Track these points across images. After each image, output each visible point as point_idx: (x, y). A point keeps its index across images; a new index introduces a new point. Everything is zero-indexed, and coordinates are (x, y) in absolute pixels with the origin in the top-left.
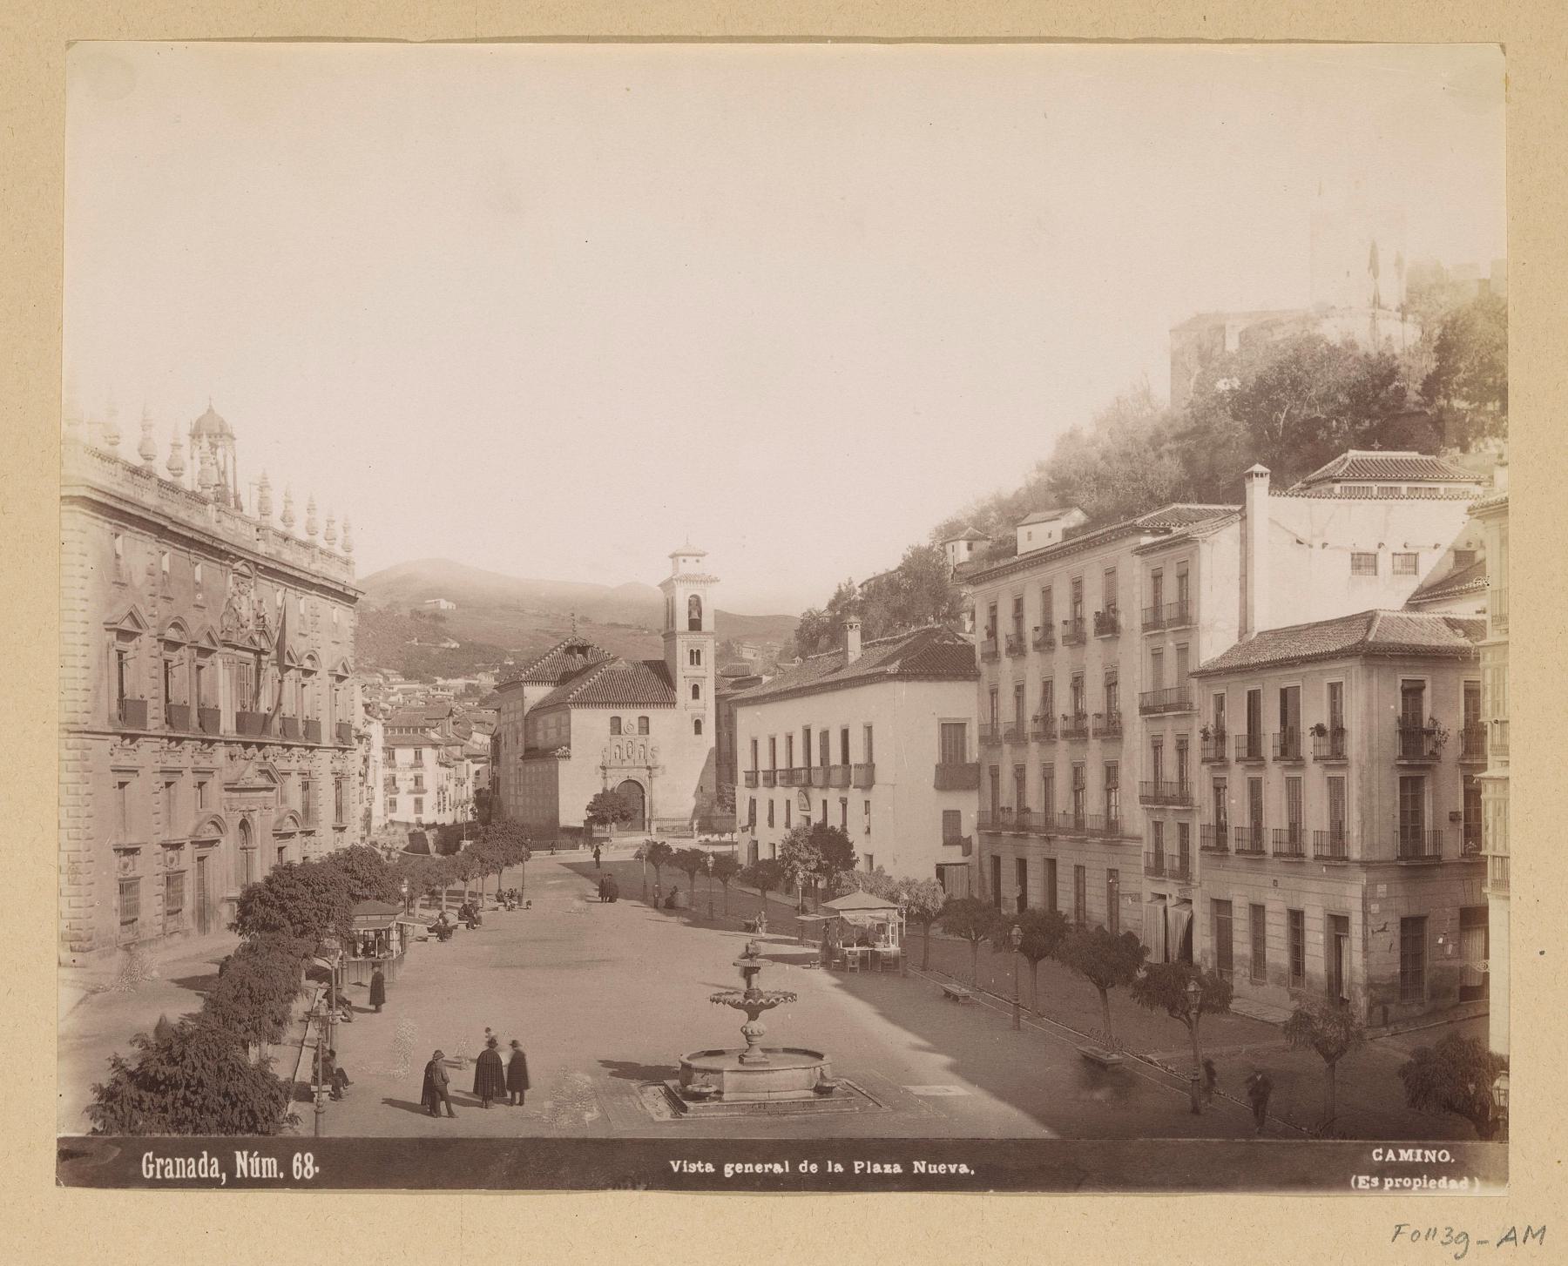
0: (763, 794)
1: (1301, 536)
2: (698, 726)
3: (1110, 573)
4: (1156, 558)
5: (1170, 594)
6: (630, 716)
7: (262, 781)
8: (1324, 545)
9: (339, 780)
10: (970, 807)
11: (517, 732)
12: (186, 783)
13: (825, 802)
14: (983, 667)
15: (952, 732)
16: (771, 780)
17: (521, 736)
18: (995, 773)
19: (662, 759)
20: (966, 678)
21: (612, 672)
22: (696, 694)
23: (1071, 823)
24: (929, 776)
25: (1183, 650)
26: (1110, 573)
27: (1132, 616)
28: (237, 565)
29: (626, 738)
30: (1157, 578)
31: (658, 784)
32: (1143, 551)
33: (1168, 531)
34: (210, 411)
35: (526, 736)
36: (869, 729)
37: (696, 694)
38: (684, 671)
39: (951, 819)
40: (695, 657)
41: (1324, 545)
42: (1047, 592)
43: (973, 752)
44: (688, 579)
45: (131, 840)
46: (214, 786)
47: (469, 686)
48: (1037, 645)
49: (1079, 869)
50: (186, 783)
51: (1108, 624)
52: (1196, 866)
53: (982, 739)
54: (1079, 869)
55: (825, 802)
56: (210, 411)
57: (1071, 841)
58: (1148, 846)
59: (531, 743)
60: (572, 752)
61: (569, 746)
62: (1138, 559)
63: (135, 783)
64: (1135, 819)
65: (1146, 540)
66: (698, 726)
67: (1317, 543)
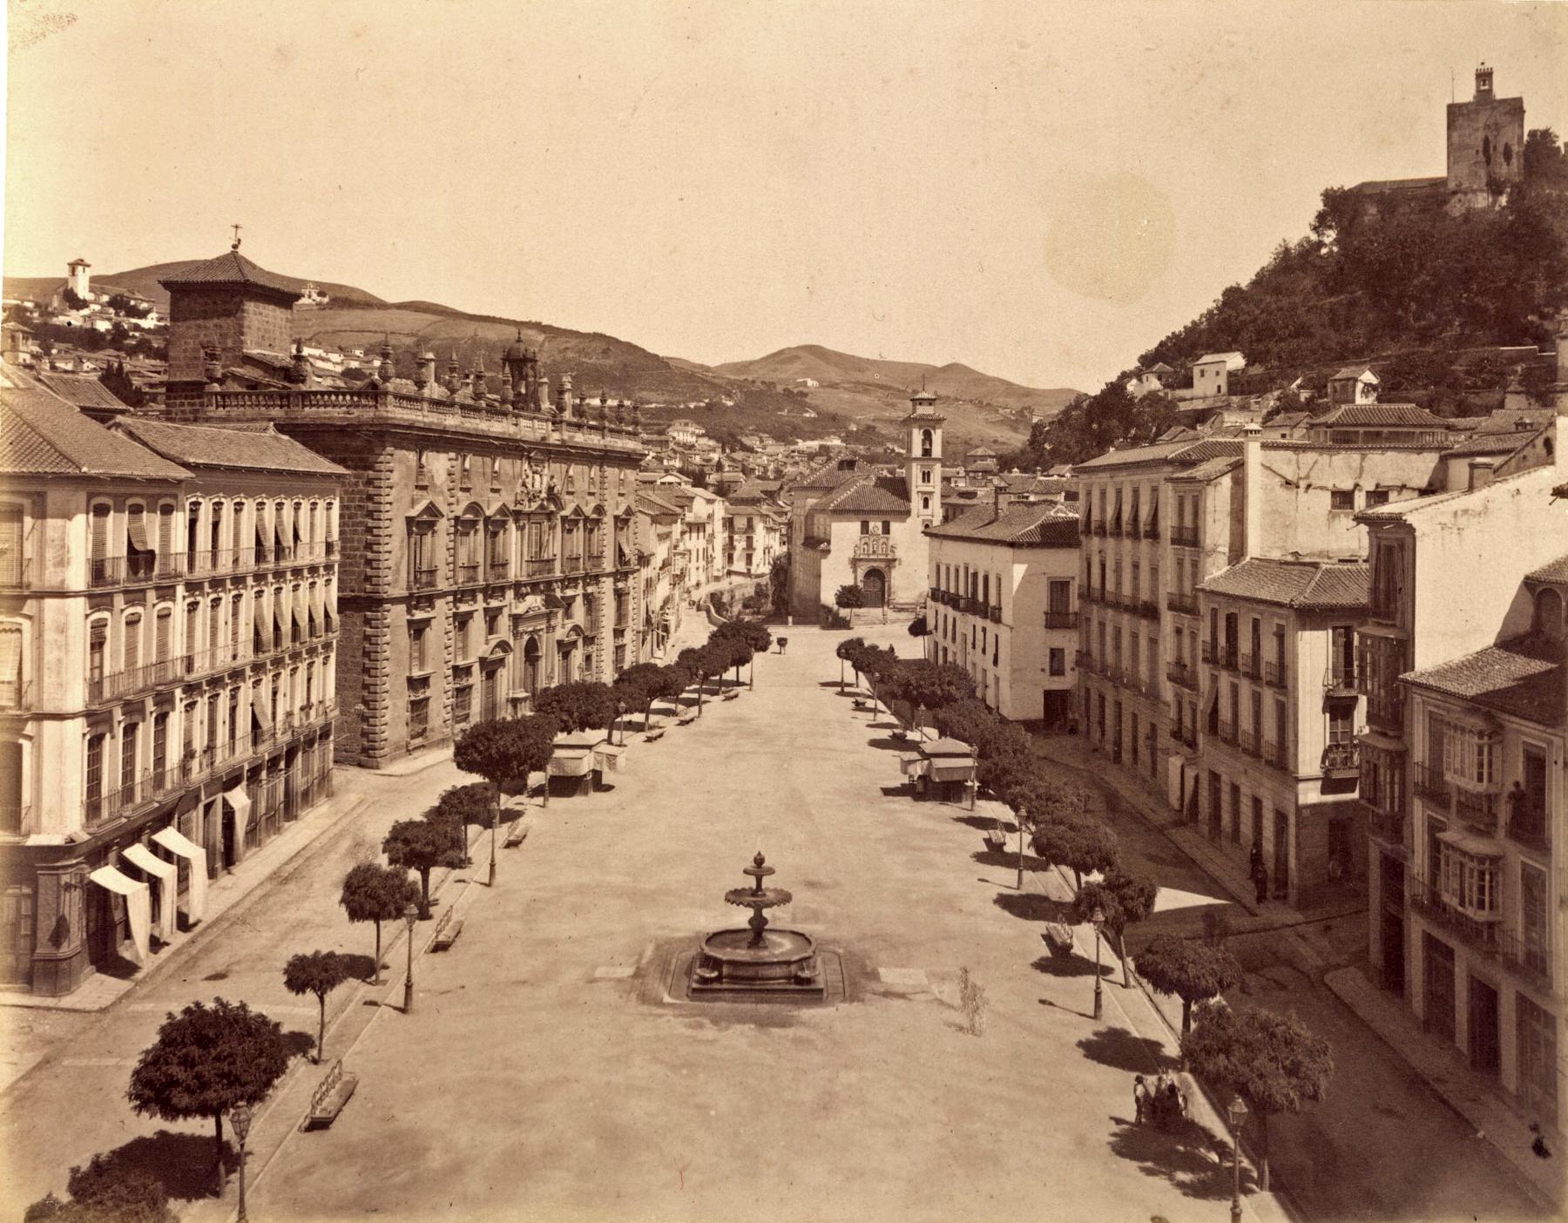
1: (1289, 478)
8: (1309, 486)
9: (620, 595)
10: (1069, 642)
12: (478, 625)
14: (1082, 538)
15: (1059, 587)
18: (1088, 620)
19: (899, 554)
20: (1070, 546)
22: (926, 505)
24: (1042, 620)
27: (1168, 523)
31: (894, 573)
37: (926, 505)
38: (916, 485)
39: (1056, 654)
40: (926, 477)
41: (1309, 486)
43: (1075, 604)
46: (504, 622)
47: (821, 447)
51: (1153, 534)
53: (1080, 596)
60: (832, 547)
61: (829, 542)
63: (430, 634)
67: (1303, 484)
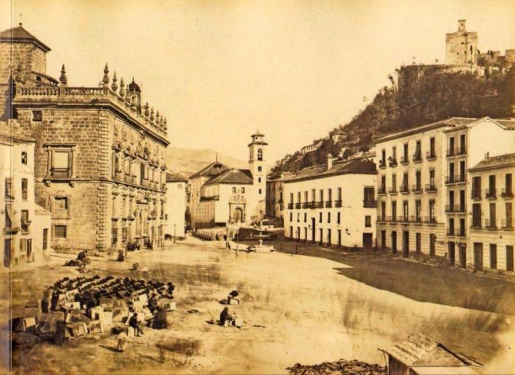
0: (295, 211)
2: (260, 191)
3: (432, 140)
4: (452, 135)
5: (458, 145)
6: (239, 187)
7: (145, 201)
11: (198, 192)
12: (128, 199)
13: (329, 214)
15: (368, 191)
16: (298, 207)
17: (199, 194)
18: (384, 204)
21: (232, 173)
23: (415, 219)
25: (463, 164)
26: (432, 140)
28: (142, 131)
29: (237, 194)
30: (452, 140)
32: (446, 132)
33: (454, 126)
34: (133, 82)
35: (201, 193)
36: (340, 189)
42: (406, 146)
44: (259, 143)
45: (115, 217)
48: (402, 162)
49: (418, 235)
50: (128, 199)
52: (468, 231)
54: (418, 235)
55: (329, 214)
56: (133, 82)
57: (459, 215)
58: (447, 225)
59: (203, 196)
62: (444, 134)
64: (442, 218)
65: (447, 128)
66: (260, 191)
